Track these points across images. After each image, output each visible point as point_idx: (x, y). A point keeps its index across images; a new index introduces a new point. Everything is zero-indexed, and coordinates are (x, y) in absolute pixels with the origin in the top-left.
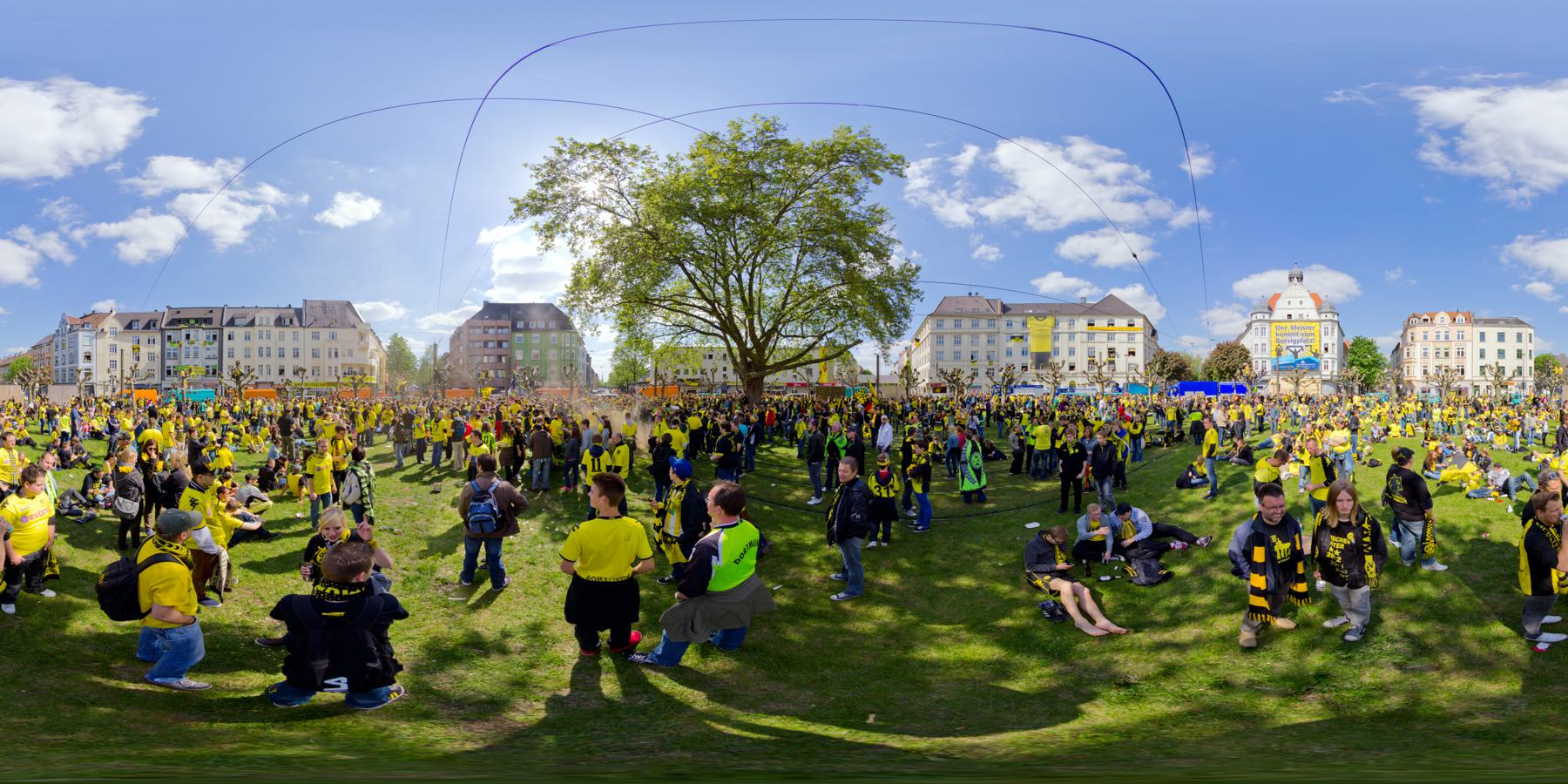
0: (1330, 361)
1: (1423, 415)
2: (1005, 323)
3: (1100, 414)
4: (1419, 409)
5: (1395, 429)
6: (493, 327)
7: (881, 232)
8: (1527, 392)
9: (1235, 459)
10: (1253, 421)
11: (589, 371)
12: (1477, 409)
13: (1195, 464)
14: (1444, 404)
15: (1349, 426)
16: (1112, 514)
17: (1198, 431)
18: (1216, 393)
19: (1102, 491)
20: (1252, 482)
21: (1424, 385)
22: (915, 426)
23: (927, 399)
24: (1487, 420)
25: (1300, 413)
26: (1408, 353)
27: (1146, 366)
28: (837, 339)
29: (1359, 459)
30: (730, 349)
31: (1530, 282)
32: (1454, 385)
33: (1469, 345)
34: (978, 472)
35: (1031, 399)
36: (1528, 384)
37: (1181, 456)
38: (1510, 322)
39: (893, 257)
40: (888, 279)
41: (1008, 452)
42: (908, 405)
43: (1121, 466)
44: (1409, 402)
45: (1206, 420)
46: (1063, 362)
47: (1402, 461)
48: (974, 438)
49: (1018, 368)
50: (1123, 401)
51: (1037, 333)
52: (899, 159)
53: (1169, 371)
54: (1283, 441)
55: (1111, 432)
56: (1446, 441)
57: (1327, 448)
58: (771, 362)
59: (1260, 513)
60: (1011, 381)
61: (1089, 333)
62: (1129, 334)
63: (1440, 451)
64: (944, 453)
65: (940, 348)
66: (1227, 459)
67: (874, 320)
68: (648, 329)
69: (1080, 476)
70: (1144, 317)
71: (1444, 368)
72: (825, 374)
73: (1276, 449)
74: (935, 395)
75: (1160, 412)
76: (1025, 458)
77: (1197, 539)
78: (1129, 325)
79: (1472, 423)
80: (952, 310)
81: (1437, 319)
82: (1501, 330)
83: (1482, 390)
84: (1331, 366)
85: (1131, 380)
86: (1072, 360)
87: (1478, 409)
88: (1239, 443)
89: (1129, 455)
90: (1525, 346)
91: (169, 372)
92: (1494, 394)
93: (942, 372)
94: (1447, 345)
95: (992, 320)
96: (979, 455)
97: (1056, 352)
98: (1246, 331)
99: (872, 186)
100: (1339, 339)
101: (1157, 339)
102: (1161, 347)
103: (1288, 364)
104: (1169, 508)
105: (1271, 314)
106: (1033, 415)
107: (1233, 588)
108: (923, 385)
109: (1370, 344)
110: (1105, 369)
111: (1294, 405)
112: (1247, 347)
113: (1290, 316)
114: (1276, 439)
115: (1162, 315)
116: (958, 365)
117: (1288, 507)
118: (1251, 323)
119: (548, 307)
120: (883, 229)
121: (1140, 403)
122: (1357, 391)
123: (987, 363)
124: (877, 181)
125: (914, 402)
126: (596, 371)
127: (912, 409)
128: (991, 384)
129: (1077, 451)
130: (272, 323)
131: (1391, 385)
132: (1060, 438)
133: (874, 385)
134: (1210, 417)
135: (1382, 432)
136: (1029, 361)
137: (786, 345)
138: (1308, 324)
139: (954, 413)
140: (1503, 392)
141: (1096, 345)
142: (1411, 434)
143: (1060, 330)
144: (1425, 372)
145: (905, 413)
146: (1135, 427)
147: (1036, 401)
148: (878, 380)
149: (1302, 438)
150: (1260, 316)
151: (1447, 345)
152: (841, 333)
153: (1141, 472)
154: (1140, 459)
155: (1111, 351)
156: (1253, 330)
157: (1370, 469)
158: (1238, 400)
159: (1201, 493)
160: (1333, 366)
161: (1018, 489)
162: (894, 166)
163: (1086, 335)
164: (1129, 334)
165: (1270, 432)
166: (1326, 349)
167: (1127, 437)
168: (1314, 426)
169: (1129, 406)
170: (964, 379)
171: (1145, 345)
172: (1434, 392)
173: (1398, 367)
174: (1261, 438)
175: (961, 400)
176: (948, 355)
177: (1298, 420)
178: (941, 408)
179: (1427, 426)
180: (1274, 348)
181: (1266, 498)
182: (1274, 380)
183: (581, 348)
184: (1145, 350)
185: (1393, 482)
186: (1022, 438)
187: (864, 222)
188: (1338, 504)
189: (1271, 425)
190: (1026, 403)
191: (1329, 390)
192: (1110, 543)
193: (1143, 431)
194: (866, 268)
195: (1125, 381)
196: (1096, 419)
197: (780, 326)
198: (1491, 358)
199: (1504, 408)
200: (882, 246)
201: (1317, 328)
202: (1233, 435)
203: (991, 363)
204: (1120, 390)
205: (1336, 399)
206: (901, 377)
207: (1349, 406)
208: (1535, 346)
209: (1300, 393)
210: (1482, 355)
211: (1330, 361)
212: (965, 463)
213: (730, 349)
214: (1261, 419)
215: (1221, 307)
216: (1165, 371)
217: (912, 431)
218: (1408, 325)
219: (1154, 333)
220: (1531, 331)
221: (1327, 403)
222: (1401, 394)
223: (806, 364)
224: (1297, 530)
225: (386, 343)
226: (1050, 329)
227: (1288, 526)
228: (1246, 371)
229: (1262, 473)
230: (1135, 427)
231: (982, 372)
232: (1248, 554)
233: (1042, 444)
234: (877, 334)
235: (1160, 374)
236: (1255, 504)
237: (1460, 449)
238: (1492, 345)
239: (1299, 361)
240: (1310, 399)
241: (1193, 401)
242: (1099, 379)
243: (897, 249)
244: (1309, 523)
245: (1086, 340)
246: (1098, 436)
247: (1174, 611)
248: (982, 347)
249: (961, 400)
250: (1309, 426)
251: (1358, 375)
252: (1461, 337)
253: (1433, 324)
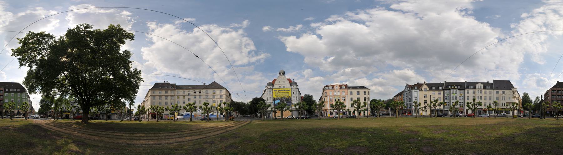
6: (560, 90)
11: (32, 107)
61: (206, 95)
70: (226, 89)
101: (231, 97)
118: (266, 90)
126: (34, 108)
130: (482, 88)
183: (29, 99)
225: (522, 95)
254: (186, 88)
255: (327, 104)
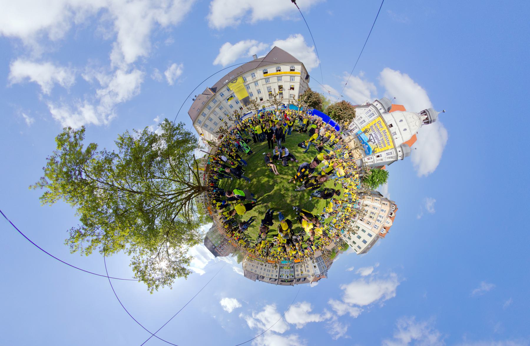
0: (372, 160)
1: (350, 201)
2: (220, 96)
3: (277, 117)
4: (353, 200)
5: (347, 191)
7: (138, 138)
8: (342, 236)
9: (317, 147)
10: (331, 142)
12: (346, 219)
13: (306, 141)
14: (352, 209)
15: (346, 175)
16: (281, 149)
17: (312, 131)
18: (327, 122)
19: (278, 142)
20: (316, 156)
21: (361, 204)
22: (226, 150)
23: (221, 142)
24: (342, 220)
25: (345, 155)
26: (377, 200)
27: (299, 96)
28: (191, 163)
29: (336, 180)
30: (195, 197)
31: (373, 272)
32: (358, 215)
33: (370, 228)
34: (247, 147)
35: (250, 119)
36: (344, 238)
37: (303, 137)
38: (367, 249)
39: (156, 132)
40: (169, 138)
41: (251, 138)
42: (220, 148)
43: (284, 135)
44: (356, 197)
45: (317, 130)
46: (257, 98)
47: (336, 193)
48: (240, 140)
49: (239, 110)
50: (287, 112)
51: (237, 90)
52: (61, 140)
53: (311, 102)
54: (332, 155)
55: (281, 124)
56: (341, 206)
57: (337, 169)
58: (197, 184)
59: (311, 163)
60: (239, 116)
61: (265, 79)
62: (291, 76)
63: (338, 204)
64: (237, 149)
65: (209, 128)
66: (315, 146)
67: (187, 148)
68: (196, 219)
69: (272, 139)
70: (303, 65)
71: (366, 213)
72: (202, 169)
73: (328, 155)
74: (222, 140)
75: (301, 119)
76: (256, 138)
77: (296, 160)
78: (291, 70)
79: (343, 216)
80: (195, 113)
81: (389, 220)
82: (367, 244)
83: (351, 223)
84: (370, 161)
85: (291, 103)
86: (260, 96)
87: (347, 219)
88: (322, 144)
89: (287, 132)
90: (355, 247)
91: (292, 267)
92: (348, 226)
93: (217, 132)
94: (375, 219)
95: (213, 99)
96: (245, 143)
97: (251, 95)
98: (364, 106)
99: (99, 149)
100: (385, 163)
101: (309, 82)
102: (310, 87)
103: (362, 139)
104: (294, 150)
105: (385, 112)
106: (253, 124)
107: (295, 172)
108: (217, 141)
109: (384, 181)
110: (278, 97)
111: (346, 152)
112: (356, 114)
113: (391, 126)
114: (332, 153)
115: (316, 65)
116: (219, 126)
117: (316, 168)
118: (370, 105)
119: (205, 245)
120: (136, 137)
121: (294, 114)
122: (360, 175)
123: (227, 116)
124: (94, 147)
125: (220, 146)
127: (222, 148)
128: (233, 122)
129: (270, 131)
130: (265, 278)
131: (363, 190)
132: (264, 128)
133: (209, 155)
134: (319, 129)
135: (346, 186)
136: (241, 105)
137: (192, 180)
138: (390, 140)
139: (231, 139)
140: (347, 229)
141: (271, 85)
142: (345, 196)
143: (248, 83)
144: (367, 205)
145: (221, 150)
146: (290, 123)
147: (252, 118)
148: (209, 153)
149: (336, 160)
150: (379, 106)
151: (375, 219)
152: (189, 161)
153: (290, 138)
154: (290, 134)
155: (280, 87)
156: (367, 109)
157: (334, 184)
158: (333, 131)
159: (303, 150)
160: (370, 162)
161: (258, 146)
162: (72, 139)
163: (264, 80)
164: (291, 76)
165: (332, 149)
166: (378, 156)
167: (287, 126)
168: (342, 162)
169: (289, 114)
170: (224, 128)
171: (300, 84)
172: (358, 206)
173: (371, 194)
174: (328, 148)
175: (229, 134)
176: (213, 127)
177: (342, 156)
178: (227, 141)
179: (346, 201)
180: (366, 128)
181: (315, 162)
182: (351, 137)
184: (300, 87)
185: (330, 190)
186: (253, 132)
187: (131, 149)
188: (322, 178)
189: (335, 148)
190: (249, 121)
191: (358, 163)
192: (279, 156)
193: (293, 125)
194: (161, 147)
195: (288, 103)
196: (276, 119)
197: (186, 182)
198: (360, 233)
199: (342, 227)
200: (148, 138)
201: (390, 147)
202: (322, 140)
203: (228, 115)
204: (285, 107)
205: (355, 167)
206: (211, 146)
207: (354, 173)
208: (352, 249)
209: (352, 152)
210: (363, 230)
211: (372, 160)
212: (243, 147)
213: (195, 197)
214: (334, 144)
215: (362, 79)
216: (309, 101)
217: (227, 152)
218: (392, 203)
219: (307, 77)
220: (358, 253)
221: (353, 164)
222: (360, 194)
223: (198, 174)
224: (312, 173)
225: (241, 263)
226: (242, 84)
227: (312, 170)
228: (346, 124)
229: (320, 156)
230: (290, 123)
231: (228, 121)
232: (302, 169)
233: (259, 132)
234: (193, 148)
235: (306, 102)
236: (312, 161)
237: (337, 209)
238: (364, 236)
239: (367, 144)
240: (352, 157)
241: (316, 120)
242: (275, 102)
243: (151, 129)
244: (315, 174)
245: (265, 83)
246: (277, 126)
247: (286, 172)
248: (220, 113)
249: (229, 134)
250: (342, 160)
251: (368, 175)
252: (375, 227)
253: (388, 217)
254: (227, 81)
255: (379, 203)
